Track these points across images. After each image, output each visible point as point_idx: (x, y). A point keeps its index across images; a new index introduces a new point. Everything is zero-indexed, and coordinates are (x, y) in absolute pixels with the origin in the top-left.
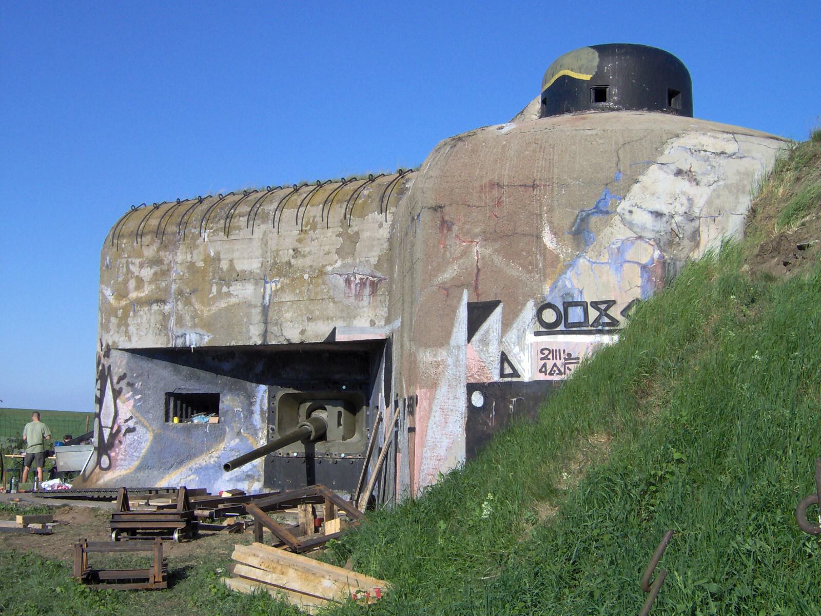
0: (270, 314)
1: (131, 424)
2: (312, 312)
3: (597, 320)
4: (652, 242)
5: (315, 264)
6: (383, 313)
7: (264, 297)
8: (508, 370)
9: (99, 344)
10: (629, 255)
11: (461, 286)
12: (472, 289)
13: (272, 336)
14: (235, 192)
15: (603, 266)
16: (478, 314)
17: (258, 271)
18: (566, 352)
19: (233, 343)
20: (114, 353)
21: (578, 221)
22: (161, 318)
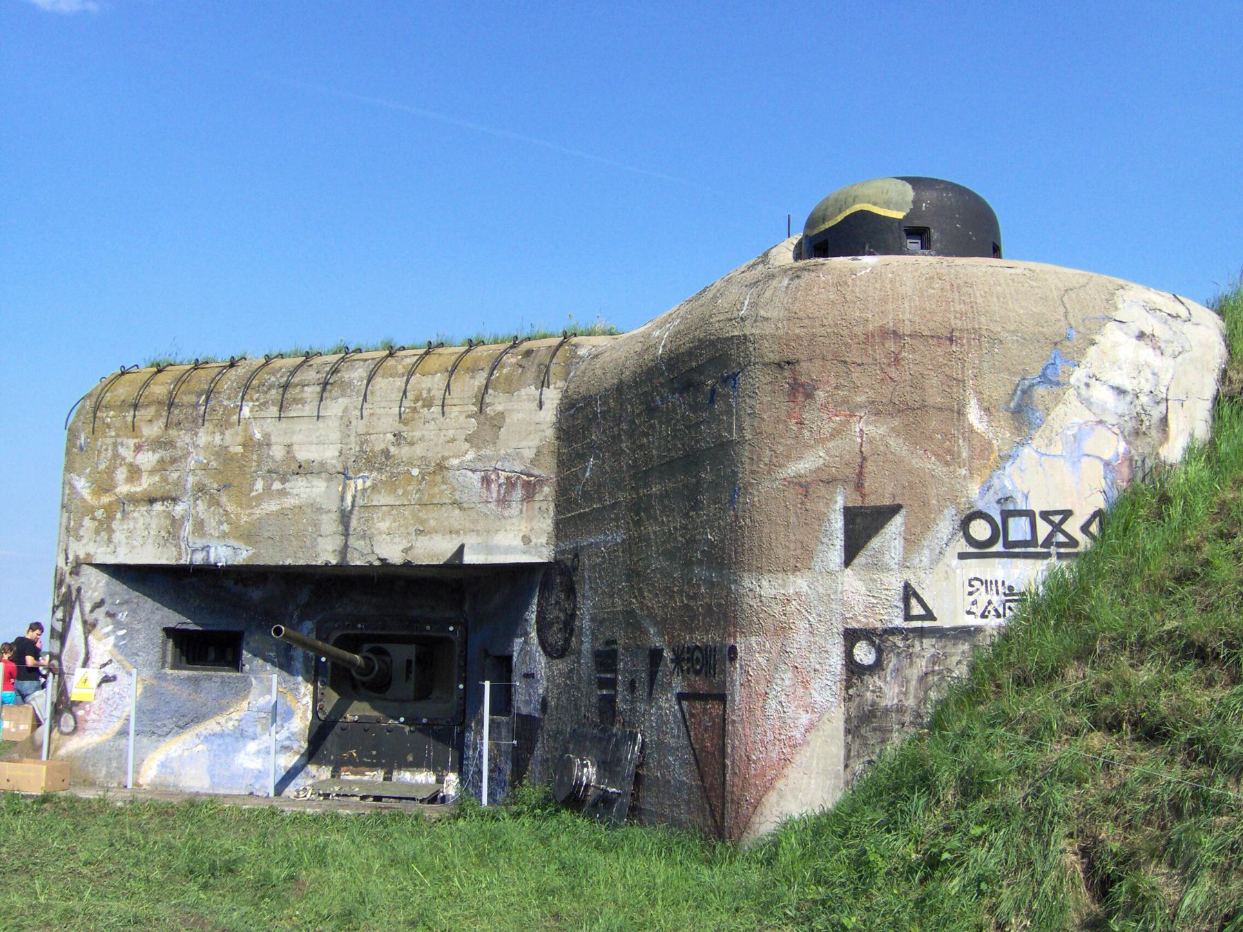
0: (354, 523)
1: (110, 671)
2: (422, 522)
3: (1048, 542)
4: (1116, 430)
5: (430, 455)
6: (544, 526)
7: (343, 499)
8: (917, 610)
9: (63, 556)
10: (1088, 447)
11: (831, 482)
12: (852, 486)
13: (356, 555)
14: (283, 352)
15: (1055, 459)
16: (863, 526)
17: (334, 462)
18: (1007, 584)
19: (289, 562)
20: (87, 570)
21: (1019, 392)
22: (168, 522)
